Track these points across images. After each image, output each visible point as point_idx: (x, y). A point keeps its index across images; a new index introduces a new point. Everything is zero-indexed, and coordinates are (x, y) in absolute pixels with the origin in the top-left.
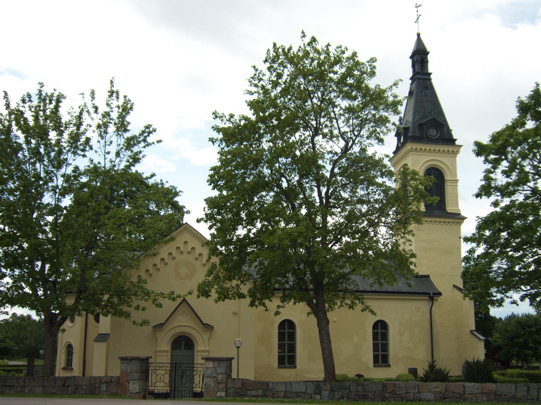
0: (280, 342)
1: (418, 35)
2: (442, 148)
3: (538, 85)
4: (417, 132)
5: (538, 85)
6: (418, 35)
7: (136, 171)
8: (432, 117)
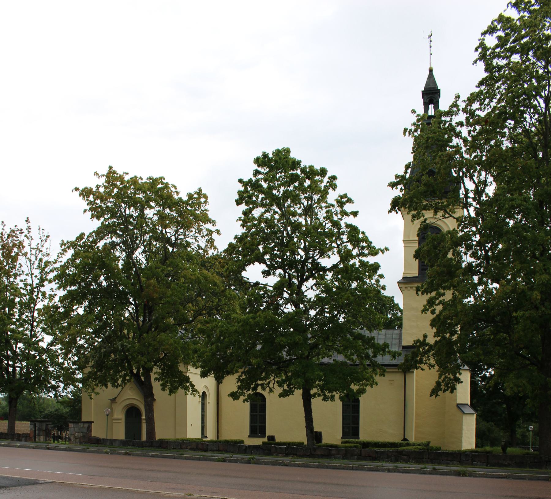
1: (431, 71)
3: (77, 189)
5: (77, 189)
6: (431, 71)
7: (65, 246)
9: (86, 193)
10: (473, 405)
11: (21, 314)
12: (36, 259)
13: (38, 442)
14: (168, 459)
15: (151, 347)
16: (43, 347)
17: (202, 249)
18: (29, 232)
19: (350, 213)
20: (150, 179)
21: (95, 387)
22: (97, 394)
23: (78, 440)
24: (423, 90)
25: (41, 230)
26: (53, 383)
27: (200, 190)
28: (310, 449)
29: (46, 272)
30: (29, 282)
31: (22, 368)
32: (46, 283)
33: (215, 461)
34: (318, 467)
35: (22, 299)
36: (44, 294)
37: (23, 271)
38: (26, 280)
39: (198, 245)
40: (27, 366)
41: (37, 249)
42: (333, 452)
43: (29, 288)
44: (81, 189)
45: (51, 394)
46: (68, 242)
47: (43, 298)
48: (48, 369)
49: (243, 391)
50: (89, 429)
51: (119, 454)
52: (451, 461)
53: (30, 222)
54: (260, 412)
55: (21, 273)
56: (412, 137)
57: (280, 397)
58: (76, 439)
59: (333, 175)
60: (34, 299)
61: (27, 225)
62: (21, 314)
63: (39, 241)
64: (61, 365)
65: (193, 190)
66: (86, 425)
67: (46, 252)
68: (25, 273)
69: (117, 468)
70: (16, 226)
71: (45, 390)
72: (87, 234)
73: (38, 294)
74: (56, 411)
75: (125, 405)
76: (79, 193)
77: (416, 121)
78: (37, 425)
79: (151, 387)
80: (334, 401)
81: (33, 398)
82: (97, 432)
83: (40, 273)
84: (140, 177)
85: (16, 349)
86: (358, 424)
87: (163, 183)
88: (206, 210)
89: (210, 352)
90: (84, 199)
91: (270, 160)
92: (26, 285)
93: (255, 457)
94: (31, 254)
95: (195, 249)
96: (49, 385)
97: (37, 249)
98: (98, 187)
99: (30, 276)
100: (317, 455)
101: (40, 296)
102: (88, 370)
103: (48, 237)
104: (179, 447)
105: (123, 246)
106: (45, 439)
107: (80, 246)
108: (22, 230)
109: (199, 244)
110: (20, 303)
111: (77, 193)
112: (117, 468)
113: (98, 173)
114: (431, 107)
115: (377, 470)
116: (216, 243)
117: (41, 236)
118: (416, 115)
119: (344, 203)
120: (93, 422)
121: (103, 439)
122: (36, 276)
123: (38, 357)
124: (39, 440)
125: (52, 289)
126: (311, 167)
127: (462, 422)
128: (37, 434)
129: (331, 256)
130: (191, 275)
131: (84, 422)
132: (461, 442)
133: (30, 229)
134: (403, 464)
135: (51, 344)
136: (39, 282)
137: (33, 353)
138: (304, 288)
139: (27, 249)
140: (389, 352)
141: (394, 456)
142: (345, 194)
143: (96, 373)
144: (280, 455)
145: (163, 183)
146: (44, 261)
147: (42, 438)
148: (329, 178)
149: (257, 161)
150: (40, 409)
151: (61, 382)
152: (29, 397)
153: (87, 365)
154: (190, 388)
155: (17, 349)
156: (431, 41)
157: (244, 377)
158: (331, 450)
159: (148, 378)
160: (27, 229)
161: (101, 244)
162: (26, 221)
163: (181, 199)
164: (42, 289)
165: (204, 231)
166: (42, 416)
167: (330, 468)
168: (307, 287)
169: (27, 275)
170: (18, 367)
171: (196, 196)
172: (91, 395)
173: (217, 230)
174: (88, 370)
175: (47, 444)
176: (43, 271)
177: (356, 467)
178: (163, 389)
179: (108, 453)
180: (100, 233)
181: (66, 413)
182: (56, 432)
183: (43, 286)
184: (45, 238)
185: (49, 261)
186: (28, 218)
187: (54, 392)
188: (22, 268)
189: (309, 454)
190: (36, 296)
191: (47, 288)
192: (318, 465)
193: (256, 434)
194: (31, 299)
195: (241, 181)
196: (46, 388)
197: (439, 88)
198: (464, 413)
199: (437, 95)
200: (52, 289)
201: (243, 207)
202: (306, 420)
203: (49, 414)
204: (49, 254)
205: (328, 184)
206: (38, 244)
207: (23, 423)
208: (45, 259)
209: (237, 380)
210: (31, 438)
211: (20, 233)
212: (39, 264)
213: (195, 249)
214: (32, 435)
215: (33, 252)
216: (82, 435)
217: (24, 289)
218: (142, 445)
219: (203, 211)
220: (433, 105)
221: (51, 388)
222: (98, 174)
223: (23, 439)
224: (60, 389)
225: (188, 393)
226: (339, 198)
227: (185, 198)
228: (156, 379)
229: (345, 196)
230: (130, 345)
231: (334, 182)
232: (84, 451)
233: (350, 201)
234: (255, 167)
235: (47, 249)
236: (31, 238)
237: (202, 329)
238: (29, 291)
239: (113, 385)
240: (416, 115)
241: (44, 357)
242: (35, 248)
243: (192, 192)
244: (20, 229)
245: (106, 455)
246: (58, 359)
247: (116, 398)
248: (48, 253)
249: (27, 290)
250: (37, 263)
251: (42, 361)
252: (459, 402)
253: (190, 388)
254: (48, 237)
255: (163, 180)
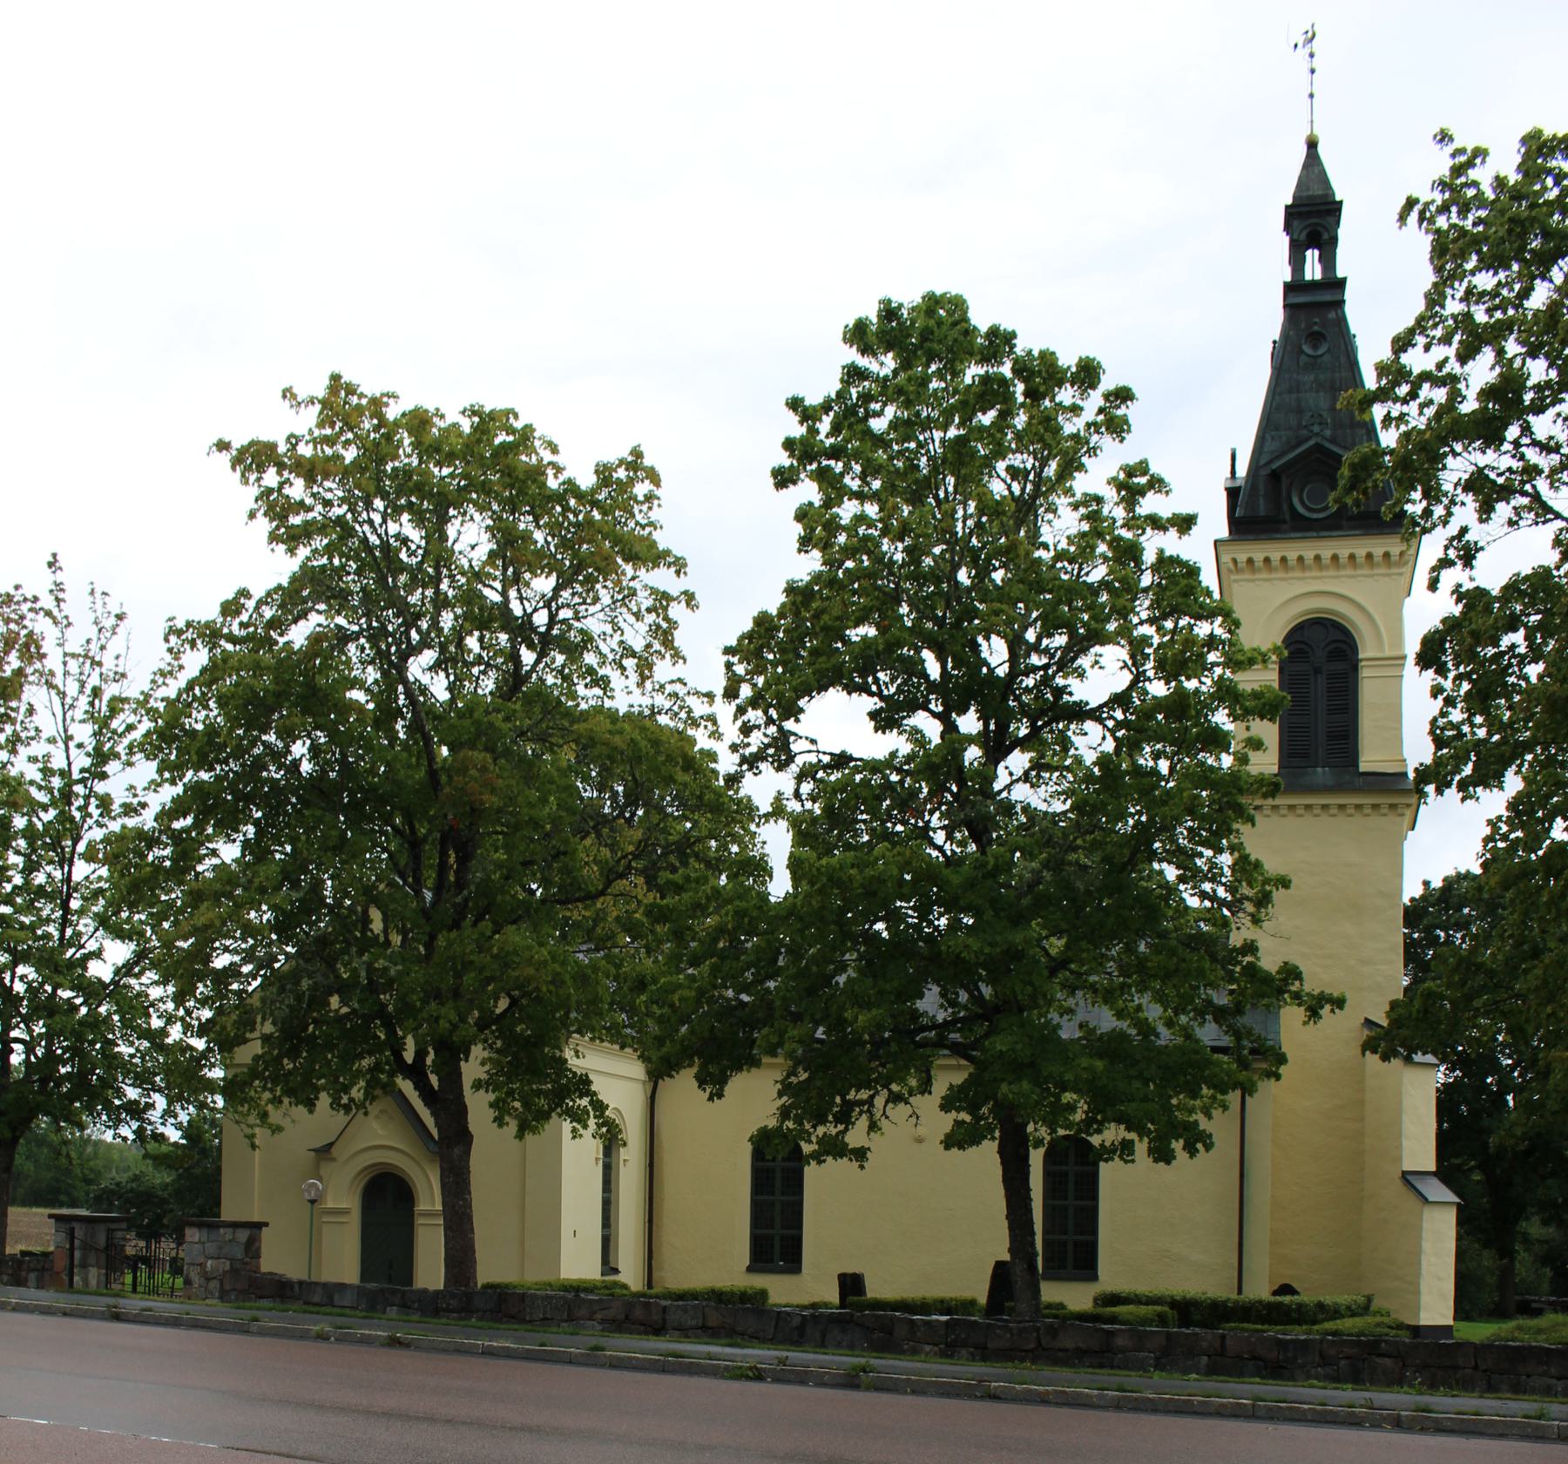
0: (758, 1231)
1: (1312, 145)
2: (1360, 546)
3: (222, 446)
4: (1261, 501)
5: (222, 446)
6: (1312, 145)
7: (183, 634)
8: (1312, 442)
9: (254, 457)
10: (1446, 1172)
11: (30, 868)
12: (81, 692)
13: (79, 1292)
14: (547, 1366)
15: (473, 975)
16: (99, 980)
17: (633, 654)
18: (58, 600)
19: (1168, 520)
20: (474, 413)
21: (270, 1107)
22: (277, 1129)
23: (214, 1285)
24: (1290, 202)
25: (98, 594)
26: (132, 1093)
27: (637, 453)
28: (1037, 1330)
29: (114, 732)
30: (58, 762)
31: (29, 1048)
32: (112, 767)
33: (723, 1377)
34: (1118, 1406)
35: (35, 819)
36: (105, 802)
37: (37, 729)
38: (47, 757)
39: (622, 642)
40: (49, 1036)
41: (86, 656)
42: (1120, 1341)
43: (56, 782)
44: (236, 444)
45: (126, 1131)
46: (189, 625)
47: (101, 815)
48: (116, 1049)
49: (801, 1124)
50: (252, 1248)
51: (366, 1341)
52: (1559, 1379)
53: (60, 568)
54: (783, 1193)
55: (32, 733)
56: (1427, 232)
57: (947, 1148)
58: (208, 1279)
59: (1121, 384)
60: (72, 819)
61: (52, 578)
62: (30, 868)
63: (92, 632)
64: (156, 1037)
65: (615, 452)
66: (243, 1235)
67: (114, 669)
68: (45, 735)
69: (387, 1415)
70: (17, 587)
71: (104, 1117)
72: (258, 592)
73: (87, 805)
74: (133, 1181)
75: (359, 1168)
76: (229, 457)
77: (1448, 174)
78: (79, 1232)
79: (463, 1110)
80: (1133, 1161)
81: (66, 1142)
82: (277, 1258)
83: (95, 734)
84: (437, 410)
85: (12, 981)
86: (1094, 1232)
87: (510, 430)
88: (651, 524)
89: (690, 988)
90: (247, 483)
91: (904, 330)
92: (47, 772)
93: (874, 1362)
94: (66, 673)
95: (611, 657)
96: (117, 1102)
97: (86, 656)
98: (293, 441)
99: (61, 744)
100: (1060, 1350)
101: (92, 809)
102: (249, 1051)
103: (120, 617)
104: (565, 1316)
105: (367, 646)
106: (103, 1279)
107: (232, 639)
108: (36, 599)
109: (624, 638)
110: (30, 833)
111: (225, 458)
112: (387, 1415)
113: (295, 390)
114: (1312, 256)
115: (1353, 1422)
116: (680, 638)
117: (99, 614)
118: (1450, 149)
119: (1141, 491)
120: (267, 1224)
121: (301, 1283)
122: (80, 746)
123: (84, 1010)
124: (86, 1281)
125: (132, 787)
126: (1048, 358)
127: (1420, 1228)
128: (76, 1262)
129: (1089, 672)
130: (610, 732)
131: (235, 1225)
132: (1417, 1293)
133: (62, 590)
134: (1421, 1394)
135: (126, 970)
136: (92, 765)
137: (65, 994)
138: (1002, 780)
139: (53, 662)
140: (1297, 996)
141: (1347, 1358)
142: (1141, 462)
143: (278, 1060)
144: (928, 1348)
145: (510, 430)
146: (106, 697)
147: (94, 1275)
148: (1107, 396)
149: (858, 335)
150: (87, 1172)
151: (160, 1090)
152: (53, 1137)
153: (248, 1035)
154: (592, 1113)
155: (17, 980)
156: (1312, 55)
157: (804, 1076)
158: (1111, 1333)
159: (452, 1078)
160: (51, 591)
161: (298, 635)
162: (50, 565)
163: (571, 487)
164: (100, 787)
165: (642, 594)
166: (92, 1195)
167: (1167, 1412)
168: (1011, 774)
169: (52, 741)
170: (17, 1040)
171: (621, 474)
172: (253, 1136)
173: (685, 593)
174: (249, 1051)
175: (111, 1301)
176: (102, 724)
177: (1270, 1409)
178: (500, 1121)
179: (328, 1339)
180: (292, 601)
181: (165, 1186)
182: (134, 1246)
183: (103, 776)
184: (112, 621)
185: (123, 696)
186: (54, 555)
187: (135, 1125)
188: (35, 718)
189: (1032, 1346)
190: (79, 809)
191: (119, 782)
192: (1119, 1399)
193: (771, 1261)
194: (64, 817)
195: (795, 404)
196: (108, 1106)
197: (1338, 198)
198: (1426, 1199)
199: (1331, 219)
200: (132, 787)
201: (808, 491)
202: (1011, 1229)
203: (112, 1191)
204: (124, 675)
205: (1101, 417)
206: (88, 641)
207: (36, 1214)
208: (111, 690)
209: (779, 1086)
210: (58, 1273)
211: (31, 610)
212: (92, 704)
213: (611, 657)
214: (61, 1263)
215: (73, 666)
216: (227, 1267)
217: (40, 788)
218: (431, 1306)
219: (643, 527)
220: (1316, 252)
221: (125, 1111)
222: (294, 396)
223: (32, 1276)
224: (155, 1115)
225: (582, 1131)
226: (1122, 476)
227: (587, 480)
228: (477, 1085)
229: (1142, 468)
230: (400, 967)
231: (1119, 412)
232: (242, 1330)
233: (1157, 484)
234: (852, 355)
235: (117, 657)
236: (65, 622)
237: (660, 908)
238: (56, 793)
239: (336, 1104)
240: (1450, 149)
241: (103, 1010)
242: (79, 655)
243: (611, 457)
244: (29, 596)
245: (323, 1345)
246: (149, 1016)
247: (332, 1144)
248: (120, 670)
249: (50, 790)
250: (83, 702)
251: (96, 1024)
252: (1408, 1166)
253: (592, 1113)
254: (120, 617)
255: (512, 420)
